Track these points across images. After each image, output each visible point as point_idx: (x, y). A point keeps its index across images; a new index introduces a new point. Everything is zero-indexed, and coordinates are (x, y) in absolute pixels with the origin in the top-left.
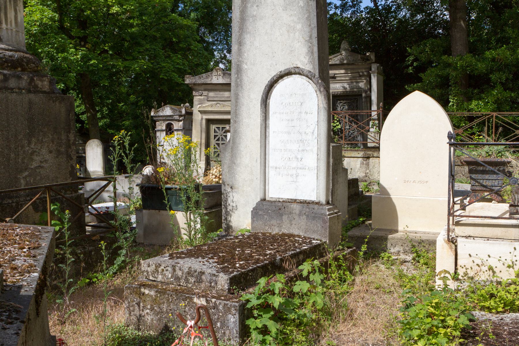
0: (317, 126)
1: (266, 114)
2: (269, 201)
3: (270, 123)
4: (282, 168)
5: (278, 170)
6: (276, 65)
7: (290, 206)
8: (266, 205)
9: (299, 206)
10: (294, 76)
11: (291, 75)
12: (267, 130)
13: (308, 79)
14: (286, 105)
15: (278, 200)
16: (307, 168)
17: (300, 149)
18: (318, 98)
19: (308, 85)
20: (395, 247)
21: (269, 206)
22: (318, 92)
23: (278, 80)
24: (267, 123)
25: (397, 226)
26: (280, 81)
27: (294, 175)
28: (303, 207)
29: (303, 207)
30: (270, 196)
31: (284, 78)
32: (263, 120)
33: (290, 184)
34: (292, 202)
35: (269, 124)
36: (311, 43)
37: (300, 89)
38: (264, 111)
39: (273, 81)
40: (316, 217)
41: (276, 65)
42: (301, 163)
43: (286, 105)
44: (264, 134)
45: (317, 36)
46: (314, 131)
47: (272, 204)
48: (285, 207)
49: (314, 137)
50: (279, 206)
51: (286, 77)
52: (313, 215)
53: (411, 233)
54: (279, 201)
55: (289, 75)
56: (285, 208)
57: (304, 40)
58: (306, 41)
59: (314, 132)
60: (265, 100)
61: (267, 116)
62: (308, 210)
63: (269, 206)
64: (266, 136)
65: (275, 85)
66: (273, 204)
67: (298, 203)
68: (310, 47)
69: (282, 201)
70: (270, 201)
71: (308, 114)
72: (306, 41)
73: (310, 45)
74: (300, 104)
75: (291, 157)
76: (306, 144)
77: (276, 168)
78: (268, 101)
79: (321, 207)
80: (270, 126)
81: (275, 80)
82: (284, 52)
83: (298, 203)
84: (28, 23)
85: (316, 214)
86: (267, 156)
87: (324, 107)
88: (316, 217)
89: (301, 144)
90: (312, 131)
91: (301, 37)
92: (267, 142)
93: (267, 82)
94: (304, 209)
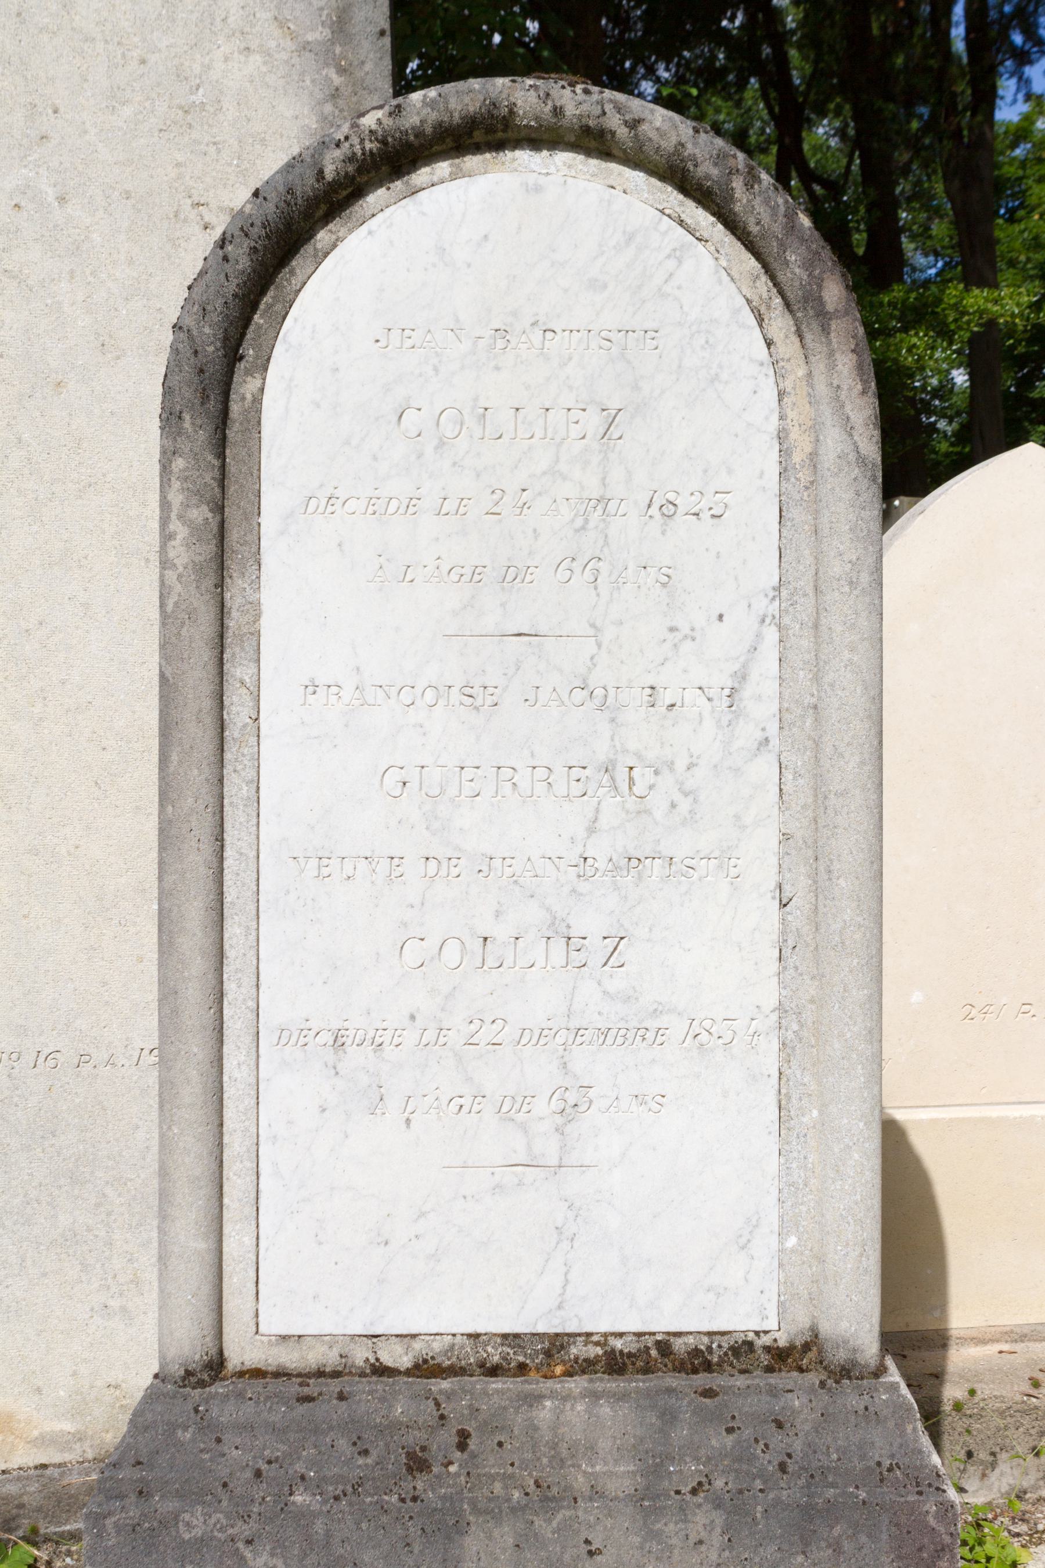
0: (771, 635)
1: (219, 508)
2: (257, 1373)
3: (268, 598)
4: (410, 1037)
5: (356, 1057)
6: (62, 200)
7: (518, 1420)
8: (247, 1428)
9: (625, 1409)
10: (523, 156)
11: (499, 146)
12: (238, 671)
13: (672, 197)
14: (449, 429)
15: (360, 1355)
16: (677, 1027)
17: (600, 849)
18: (779, 376)
19: (677, 255)
20: (993, 1465)
21: (278, 1431)
22: (780, 324)
23: (358, 193)
24: (234, 598)
25: (942, 1305)
26: (375, 198)
27: (541, 1107)
28: (669, 1417)
29: (669, 1417)
30: (273, 1323)
31: (422, 175)
32: (198, 569)
33: (498, 1188)
34: (522, 1369)
35: (255, 611)
36: (342, 71)
37: (596, 285)
38: (209, 478)
39: (307, 185)
40: (831, 1511)
41: (62, 200)
42: (617, 983)
43: (449, 429)
44: (208, 704)
45: (387, 26)
46: (742, 676)
47: (320, 1410)
48: (463, 1440)
49: (747, 734)
50: (395, 1426)
51: (443, 167)
52: (790, 1491)
53: (1023, 1338)
54: (380, 1370)
55: (477, 148)
56: (463, 1440)
57: (289, 45)
58: (305, 47)
59: (747, 692)
60: (215, 369)
61: (234, 535)
62: (719, 1441)
63: (278, 1431)
64: (222, 726)
65: (323, 237)
66: (329, 1410)
67: (587, 1367)
68: (335, 95)
69: (405, 1362)
70: (280, 1374)
71: (682, 521)
72: (305, 47)
73: (337, 80)
74: (593, 422)
75: (501, 932)
76: (658, 803)
77: (338, 1043)
78: (245, 387)
79: (851, 1398)
80: (265, 623)
81: (335, 186)
82: (127, 111)
83: (587, 1367)
84: (391, 1491)
85: (815, 1477)
86: (233, 930)
87: (861, 460)
88: (831, 1511)
89: (611, 805)
90: (720, 679)
91: (264, 15)
92: (235, 789)
93: (240, 197)
94: (681, 1433)
